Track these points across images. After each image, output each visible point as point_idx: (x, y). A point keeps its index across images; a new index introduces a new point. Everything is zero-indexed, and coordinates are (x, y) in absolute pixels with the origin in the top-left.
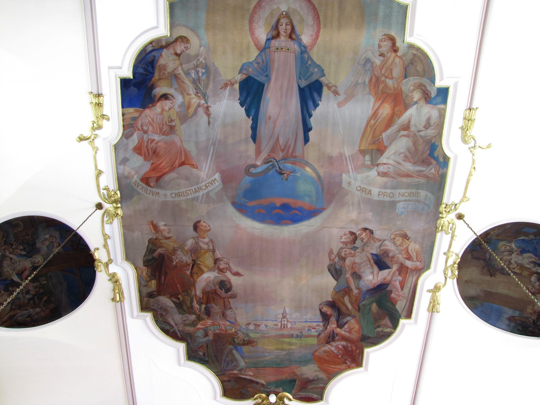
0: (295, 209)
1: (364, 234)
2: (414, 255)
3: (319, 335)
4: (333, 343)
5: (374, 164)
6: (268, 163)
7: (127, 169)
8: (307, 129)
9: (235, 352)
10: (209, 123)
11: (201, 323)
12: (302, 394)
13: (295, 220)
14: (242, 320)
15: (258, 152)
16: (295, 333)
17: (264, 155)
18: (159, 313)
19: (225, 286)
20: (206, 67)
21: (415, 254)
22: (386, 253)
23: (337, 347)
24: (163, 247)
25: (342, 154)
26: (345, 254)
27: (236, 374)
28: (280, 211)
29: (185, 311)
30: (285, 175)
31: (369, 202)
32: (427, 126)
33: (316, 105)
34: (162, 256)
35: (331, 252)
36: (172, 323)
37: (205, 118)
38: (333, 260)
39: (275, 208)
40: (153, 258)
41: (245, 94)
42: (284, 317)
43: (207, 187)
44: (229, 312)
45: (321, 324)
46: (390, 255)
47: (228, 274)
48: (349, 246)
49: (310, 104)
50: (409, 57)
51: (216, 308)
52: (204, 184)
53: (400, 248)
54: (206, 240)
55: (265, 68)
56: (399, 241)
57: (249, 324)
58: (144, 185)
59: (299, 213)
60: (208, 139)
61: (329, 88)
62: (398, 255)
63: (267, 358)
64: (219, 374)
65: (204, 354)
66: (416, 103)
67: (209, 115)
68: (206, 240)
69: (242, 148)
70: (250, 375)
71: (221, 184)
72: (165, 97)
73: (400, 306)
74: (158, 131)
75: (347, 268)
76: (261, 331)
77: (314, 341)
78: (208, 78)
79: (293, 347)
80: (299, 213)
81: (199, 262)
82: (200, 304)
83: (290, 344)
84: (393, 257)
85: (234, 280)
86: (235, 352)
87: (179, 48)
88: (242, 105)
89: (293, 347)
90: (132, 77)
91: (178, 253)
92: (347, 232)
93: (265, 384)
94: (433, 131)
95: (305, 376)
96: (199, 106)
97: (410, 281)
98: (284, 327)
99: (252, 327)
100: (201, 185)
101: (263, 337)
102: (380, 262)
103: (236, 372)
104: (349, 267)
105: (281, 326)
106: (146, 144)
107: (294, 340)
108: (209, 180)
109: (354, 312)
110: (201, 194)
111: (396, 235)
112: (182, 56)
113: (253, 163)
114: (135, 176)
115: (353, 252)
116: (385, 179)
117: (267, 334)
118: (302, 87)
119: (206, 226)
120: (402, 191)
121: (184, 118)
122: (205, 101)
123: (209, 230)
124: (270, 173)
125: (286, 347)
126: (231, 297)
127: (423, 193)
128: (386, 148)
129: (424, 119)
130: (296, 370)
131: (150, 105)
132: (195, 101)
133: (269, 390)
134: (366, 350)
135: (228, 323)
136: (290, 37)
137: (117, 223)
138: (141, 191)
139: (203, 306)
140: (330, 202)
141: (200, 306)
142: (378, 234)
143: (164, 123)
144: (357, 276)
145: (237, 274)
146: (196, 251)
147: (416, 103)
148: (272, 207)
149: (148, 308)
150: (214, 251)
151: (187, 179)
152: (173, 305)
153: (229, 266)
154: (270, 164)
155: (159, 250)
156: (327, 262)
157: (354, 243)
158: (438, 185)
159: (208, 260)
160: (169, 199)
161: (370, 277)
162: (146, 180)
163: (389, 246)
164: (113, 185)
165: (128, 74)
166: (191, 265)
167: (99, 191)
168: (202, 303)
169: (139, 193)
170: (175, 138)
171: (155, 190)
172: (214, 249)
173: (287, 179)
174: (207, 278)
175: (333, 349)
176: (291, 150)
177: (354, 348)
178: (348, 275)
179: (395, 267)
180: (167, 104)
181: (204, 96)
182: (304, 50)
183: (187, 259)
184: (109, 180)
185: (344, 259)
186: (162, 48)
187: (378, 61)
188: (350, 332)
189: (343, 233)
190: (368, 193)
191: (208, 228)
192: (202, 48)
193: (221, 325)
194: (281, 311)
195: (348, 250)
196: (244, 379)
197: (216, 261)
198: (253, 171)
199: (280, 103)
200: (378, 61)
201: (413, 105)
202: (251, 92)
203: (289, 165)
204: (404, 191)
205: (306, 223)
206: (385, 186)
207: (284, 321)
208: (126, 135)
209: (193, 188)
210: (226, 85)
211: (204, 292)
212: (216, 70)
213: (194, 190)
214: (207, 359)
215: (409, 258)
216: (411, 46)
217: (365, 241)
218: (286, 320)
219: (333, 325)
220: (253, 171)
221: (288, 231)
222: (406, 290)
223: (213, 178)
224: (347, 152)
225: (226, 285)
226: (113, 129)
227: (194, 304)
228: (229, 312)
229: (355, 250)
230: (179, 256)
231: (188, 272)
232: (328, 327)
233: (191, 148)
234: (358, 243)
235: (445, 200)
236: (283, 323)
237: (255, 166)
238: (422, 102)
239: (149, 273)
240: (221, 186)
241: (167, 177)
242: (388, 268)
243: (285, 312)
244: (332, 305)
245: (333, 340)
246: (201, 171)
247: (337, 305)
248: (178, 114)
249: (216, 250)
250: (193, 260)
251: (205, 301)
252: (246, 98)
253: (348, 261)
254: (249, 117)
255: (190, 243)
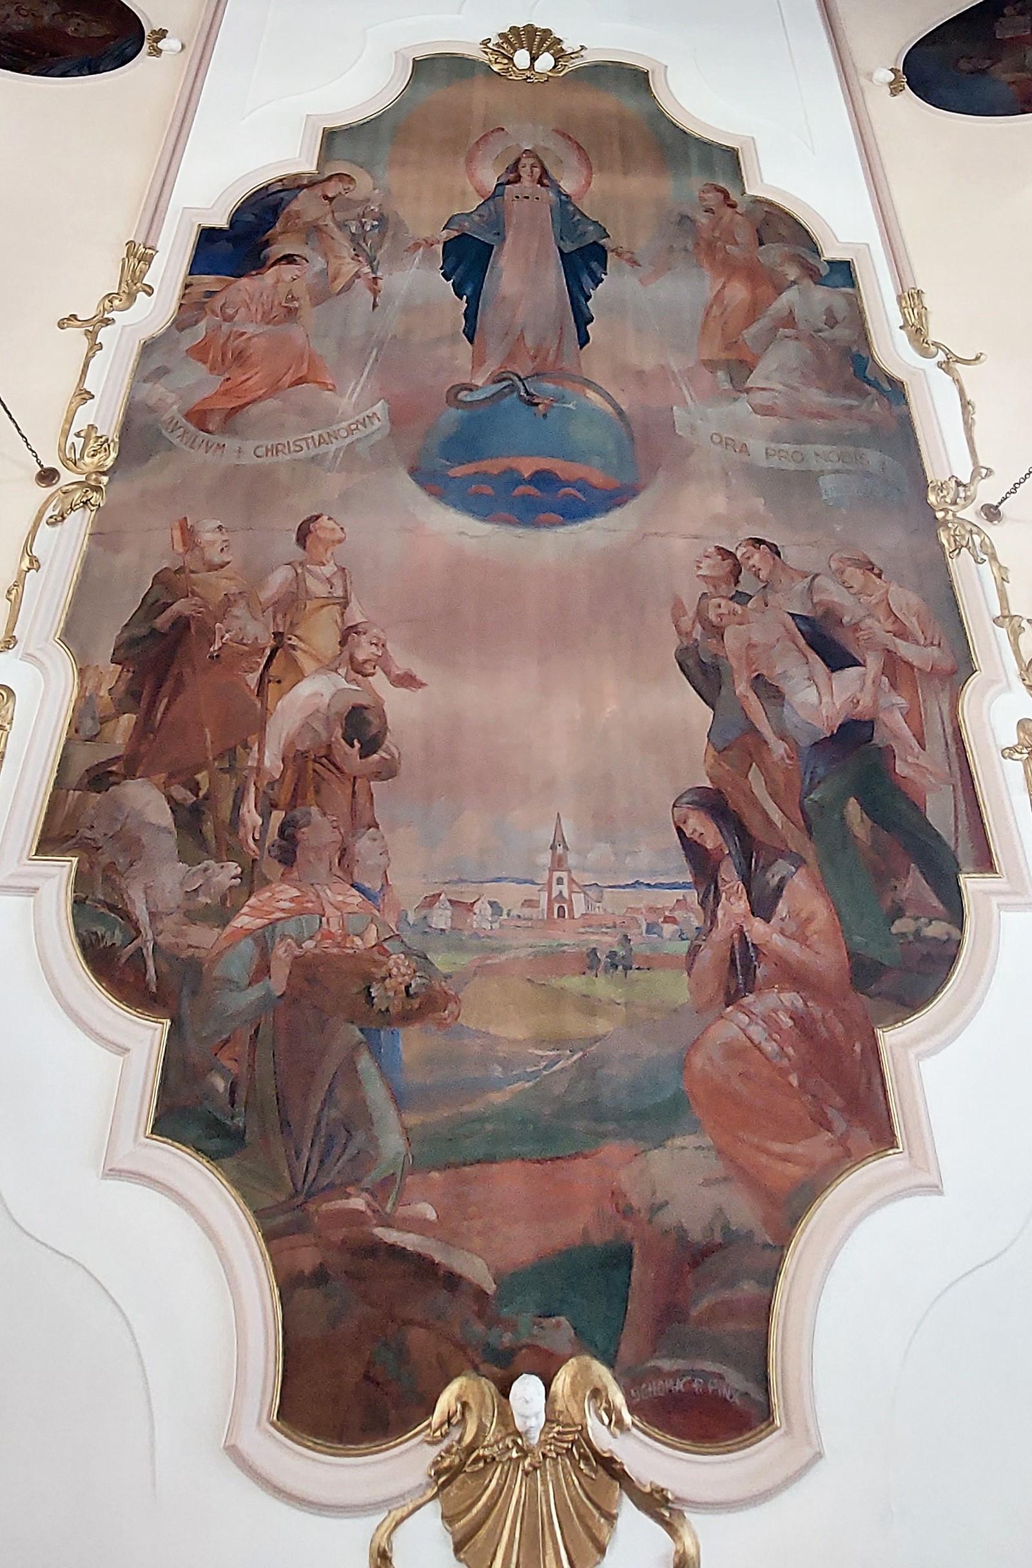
0: (569, 484)
1: (757, 556)
2: (912, 624)
3: (693, 952)
4: (751, 998)
5: (739, 386)
6: (499, 381)
7: (156, 391)
8: (582, 319)
9: (365, 1062)
10: (375, 306)
11: (252, 901)
12: (667, 1365)
13: (573, 512)
14: (408, 885)
15: (478, 361)
16: (607, 941)
17: (492, 366)
18: (105, 859)
19: (361, 726)
20: (382, 219)
21: (914, 620)
22: (831, 614)
23: (770, 1022)
24: (194, 593)
25: (663, 367)
26: (720, 615)
27: (355, 1216)
28: (532, 490)
29: (203, 844)
30: (540, 406)
31: (751, 472)
32: (832, 321)
33: (598, 281)
34: (182, 624)
35: (678, 608)
36: (141, 912)
37: (369, 296)
38: (688, 634)
39: (521, 481)
40: (153, 631)
41: (452, 260)
42: (559, 863)
43: (350, 432)
44: (363, 844)
45: (693, 896)
46: (846, 619)
47: (379, 681)
48: (724, 589)
49: (586, 280)
50: (760, 216)
51: (321, 830)
52: (344, 424)
53: (864, 599)
54: (328, 570)
55: (498, 225)
56: (855, 576)
57: (431, 901)
58: (192, 428)
59: (580, 495)
60: (369, 334)
61: (619, 255)
62: (869, 622)
63: (498, 1098)
64: (277, 1229)
65: (232, 1091)
66: (794, 282)
67: (375, 293)
68: (328, 570)
69: (444, 351)
70: (420, 1226)
71: (388, 424)
72: (289, 259)
73: (940, 811)
74: (259, 317)
75: (734, 662)
76: (476, 935)
77: (676, 988)
78: (382, 234)
79: (602, 1026)
80: (580, 495)
81: (294, 641)
82: (267, 807)
83: (590, 1006)
84: (856, 627)
85: (399, 707)
86: (365, 1062)
87: (332, 189)
88: (447, 277)
89: (602, 1026)
90: (879, 1032)
91: (236, 611)
92: (712, 550)
93: (490, 1288)
94: (847, 332)
95: (667, 1218)
96: (357, 275)
97: (935, 709)
98: (561, 913)
99: (441, 918)
100: (335, 428)
101: (482, 970)
102: (828, 644)
103: (358, 1203)
104: (739, 659)
105: (550, 909)
106: (221, 341)
107: (603, 986)
108: (360, 417)
109: (796, 840)
110: (333, 447)
111: (841, 560)
112: (334, 201)
113: (467, 381)
114: (175, 407)
115: (738, 607)
116: (773, 422)
117: (501, 950)
118: (566, 251)
119: (333, 529)
120: (821, 448)
121: (321, 296)
122: (372, 267)
123: (340, 541)
124: (506, 401)
125: (574, 1024)
126: (378, 776)
127: (873, 458)
128: (757, 358)
129: (819, 309)
130: (625, 1178)
131: (254, 273)
132: (349, 267)
133: (507, 1338)
134: (892, 1039)
135: (356, 898)
136: (540, 182)
137: (80, 523)
138: (176, 441)
139: (278, 817)
140: (654, 468)
141: (266, 816)
142: (790, 555)
143: (276, 303)
144: (769, 691)
145: (407, 681)
146: (292, 603)
147: (794, 282)
148: (512, 479)
149: (68, 838)
150: (344, 603)
151: (305, 412)
152: (165, 818)
153: (386, 652)
154: (505, 383)
155: (180, 606)
156: (671, 644)
157: (737, 582)
158: (901, 437)
159: (320, 634)
160: (249, 459)
161: (810, 695)
162: (199, 417)
163: (832, 593)
164: (110, 428)
165: (222, 222)
166: (268, 652)
167: (65, 434)
168: (274, 806)
169: (171, 447)
170: (296, 332)
171: (217, 439)
172: (345, 597)
173: (545, 416)
174: (309, 696)
175: (757, 1033)
176: (551, 358)
177: (839, 1029)
178: (742, 687)
179: (873, 663)
180: (288, 271)
181: (371, 261)
182: (565, 200)
183: (259, 631)
184: (105, 414)
185: (717, 631)
186: (301, 187)
187: (703, 219)
188: (802, 938)
189: (701, 551)
190: (741, 451)
191: (339, 535)
192: (377, 191)
193: (330, 911)
194: (547, 835)
195: (723, 602)
196: (396, 1252)
197: (348, 633)
198: (463, 395)
199: (524, 277)
200: (703, 219)
201: (789, 287)
202: (467, 259)
203: (549, 386)
204: (828, 448)
205: (599, 521)
206: (776, 437)
207: (560, 881)
208: (181, 323)
209: (316, 434)
210: (417, 246)
211: (295, 758)
212: (400, 223)
213: (317, 438)
214: (239, 1121)
215: (902, 634)
216: (757, 201)
217: (763, 574)
218: (564, 875)
219: (734, 905)
220: (463, 395)
221: (553, 545)
222: (935, 747)
223: (369, 412)
224: (675, 363)
225: (370, 723)
226: (152, 313)
227: (244, 810)
228: (363, 844)
229: (743, 604)
230: (235, 625)
231: (253, 679)
232: (720, 914)
233: (325, 349)
234: (746, 584)
235: (934, 472)
236: (556, 889)
237: (470, 388)
238: (807, 282)
239: (122, 687)
240: (388, 431)
241: (254, 410)
242: (856, 663)
243: (558, 842)
244: (714, 803)
245: (750, 986)
246: (342, 395)
247: (731, 806)
248: (310, 290)
249: (353, 598)
250: (278, 635)
251: (284, 796)
252: (454, 269)
253: (732, 639)
254: (461, 298)
255: (279, 578)
